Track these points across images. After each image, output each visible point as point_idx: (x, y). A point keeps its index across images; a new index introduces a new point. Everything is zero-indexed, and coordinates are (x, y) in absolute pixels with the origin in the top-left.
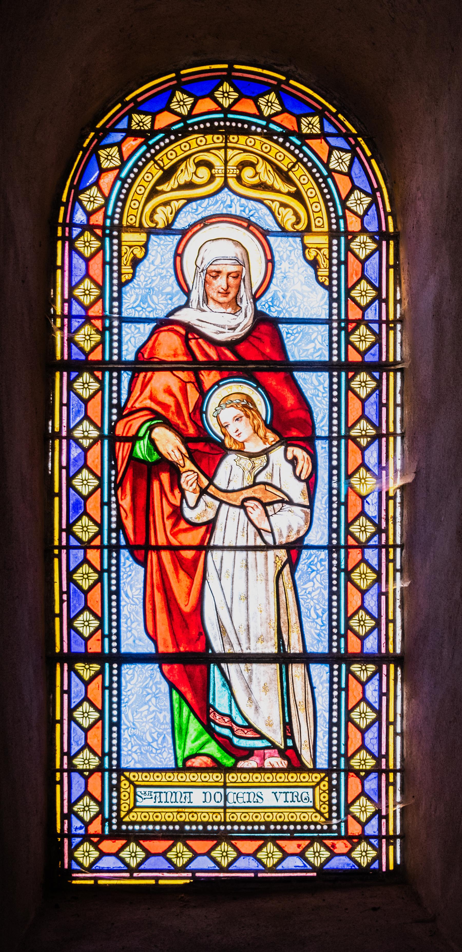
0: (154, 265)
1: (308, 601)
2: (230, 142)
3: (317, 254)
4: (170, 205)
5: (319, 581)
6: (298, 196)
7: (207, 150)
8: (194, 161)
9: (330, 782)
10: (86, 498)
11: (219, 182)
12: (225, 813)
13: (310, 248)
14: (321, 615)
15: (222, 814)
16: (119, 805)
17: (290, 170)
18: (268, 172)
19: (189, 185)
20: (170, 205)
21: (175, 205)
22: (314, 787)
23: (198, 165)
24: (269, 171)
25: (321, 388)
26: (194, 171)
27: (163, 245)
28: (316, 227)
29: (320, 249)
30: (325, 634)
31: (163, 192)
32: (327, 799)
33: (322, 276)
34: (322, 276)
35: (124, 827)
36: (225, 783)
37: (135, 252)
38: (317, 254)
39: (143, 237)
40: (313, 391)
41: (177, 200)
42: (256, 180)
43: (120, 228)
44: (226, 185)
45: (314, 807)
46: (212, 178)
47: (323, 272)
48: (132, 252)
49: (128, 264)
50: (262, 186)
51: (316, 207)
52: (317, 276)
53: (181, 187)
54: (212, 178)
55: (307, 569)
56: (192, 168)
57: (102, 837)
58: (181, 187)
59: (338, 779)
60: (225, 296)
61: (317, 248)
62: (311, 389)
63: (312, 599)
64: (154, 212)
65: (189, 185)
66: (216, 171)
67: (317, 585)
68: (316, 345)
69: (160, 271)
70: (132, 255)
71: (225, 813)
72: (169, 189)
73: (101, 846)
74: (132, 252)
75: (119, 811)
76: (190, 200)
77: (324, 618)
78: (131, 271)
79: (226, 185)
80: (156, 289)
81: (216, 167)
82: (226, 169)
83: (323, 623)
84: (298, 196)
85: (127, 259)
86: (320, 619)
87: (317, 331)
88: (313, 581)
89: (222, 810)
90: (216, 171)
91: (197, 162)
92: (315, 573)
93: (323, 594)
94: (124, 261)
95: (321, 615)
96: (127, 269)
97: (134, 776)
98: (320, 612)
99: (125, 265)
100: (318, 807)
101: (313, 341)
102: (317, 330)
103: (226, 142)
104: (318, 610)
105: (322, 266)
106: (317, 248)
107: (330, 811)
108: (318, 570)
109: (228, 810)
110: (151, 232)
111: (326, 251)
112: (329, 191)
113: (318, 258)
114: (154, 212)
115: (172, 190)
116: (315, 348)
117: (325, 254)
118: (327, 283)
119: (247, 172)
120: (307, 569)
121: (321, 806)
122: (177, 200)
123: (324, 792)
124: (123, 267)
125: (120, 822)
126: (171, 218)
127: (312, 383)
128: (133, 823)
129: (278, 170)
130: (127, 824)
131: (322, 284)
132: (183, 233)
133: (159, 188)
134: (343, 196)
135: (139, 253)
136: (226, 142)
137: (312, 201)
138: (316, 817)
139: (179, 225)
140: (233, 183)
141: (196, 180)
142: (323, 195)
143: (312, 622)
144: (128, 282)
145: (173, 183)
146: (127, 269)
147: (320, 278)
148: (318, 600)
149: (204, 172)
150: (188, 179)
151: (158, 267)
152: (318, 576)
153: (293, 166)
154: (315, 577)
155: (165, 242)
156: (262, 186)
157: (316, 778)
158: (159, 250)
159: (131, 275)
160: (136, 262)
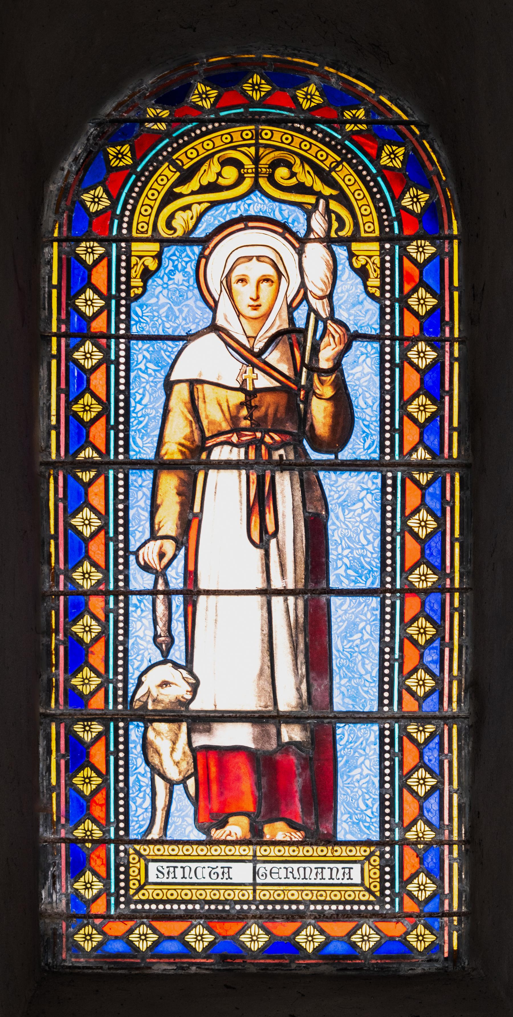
0: (141, 404)
1: (356, 790)
2: (263, 139)
3: (367, 262)
4: (191, 210)
5: (369, 632)
6: (343, 199)
7: (234, 148)
8: (218, 159)
9: (382, 856)
10: (87, 541)
11: (247, 183)
12: (254, 891)
13: (358, 256)
14: (372, 540)
15: (251, 892)
16: (127, 881)
17: (334, 169)
18: (307, 174)
19: (213, 187)
20: (191, 210)
21: (197, 209)
22: (362, 884)
23: (224, 163)
24: (309, 172)
25: (370, 548)
26: (218, 171)
27: (152, 382)
28: (365, 232)
29: (370, 257)
30: (375, 827)
31: (181, 195)
32: (378, 875)
33: (371, 287)
34: (371, 287)
35: (132, 907)
36: (255, 855)
37: (146, 263)
38: (367, 262)
39: (156, 247)
40: (360, 551)
41: (200, 203)
42: (293, 181)
43: (130, 240)
44: (256, 186)
45: (362, 884)
46: (240, 180)
47: (374, 282)
48: (143, 263)
49: (138, 276)
50: (301, 188)
51: (366, 210)
52: (366, 287)
53: (203, 190)
54: (240, 180)
55: (356, 488)
56: (216, 167)
57: (107, 917)
58: (203, 190)
59: (392, 853)
60: (255, 309)
61: (367, 256)
62: (357, 549)
63: (361, 522)
64: (172, 217)
65: (213, 187)
66: (245, 171)
67: (368, 506)
68: (362, 770)
69: (148, 411)
70: (143, 267)
71: (254, 891)
72: (189, 191)
73: (106, 929)
74: (143, 263)
75: (127, 888)
76: (214, 204)
77: (374, 810)
78: (141, 284)
79: (256, 186)
80: (143, 431)
81: (246, 167)
82: (256, 168)
83: (374, 550)
84: (343, 199)
85: (136, 272)
86: (371, 546)
87: (367, 354)
88: (362, 633)
89: (251, 888)
90: (245, 171)
91: (223, 161)
92: (364, 356)
93: (373, 380)
94: (133, 274)
95: (372, 540)
96: (136, 282)
97: (145, 850)
98: (370, 402)
99: (135, 278)
100: (367, 885)
101: (361, 500)
102: (365, 352)
103: (257, 139)
104: (369, 534)
105: (371, 276)
106: (367, 256)
107: (383, 889)
108: (367, 754)
109: (258, 887)
110: (165, 242)
111: (377, 260)
112: (381, 197)
113: (368, 267)
114: (172, 217)
115: (193, 193)
116: (361, 774)
117: (375, 262)
118: (378, 294)
119: (281, 173)
120: (356, 488)
121: (370, 884)
122: (200, 203)
123: (375, 867)
124: (132, 280)
125: (128, 902)
126: (191, 224)
127: (359, 541)
128: (143, 902)
129: (318, 171)
130: (136, 902)
131: (372, 296)
132: (204, 242)
133: (177, 190)
134: (406, 397)
135: (152, 265)
136: (257, 139)
137: (360, 203)
138: (364, 895)
139: (199, 233)
140: (264, 183)
141: (221, 181)
142: (373, 195)
143: (361, 549)
144: (138, 297)
145: (194, 185)
146: (136, 282)
147: (369, 288)
148: (368, 523)
149: (231, 174)
150: (212, 180)
151: (146, 406)
152: (368, 360)
153: (337, 166)
154: (363, 763)
155: (155, 378)
156: (301, 188)
157: (365, 851)
158: (148, 387)
159: (141, 289)
160: (147, 274)
